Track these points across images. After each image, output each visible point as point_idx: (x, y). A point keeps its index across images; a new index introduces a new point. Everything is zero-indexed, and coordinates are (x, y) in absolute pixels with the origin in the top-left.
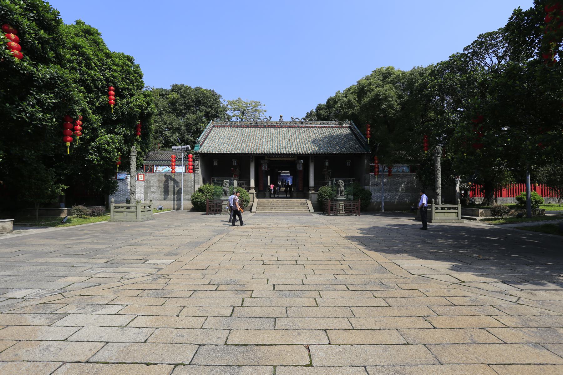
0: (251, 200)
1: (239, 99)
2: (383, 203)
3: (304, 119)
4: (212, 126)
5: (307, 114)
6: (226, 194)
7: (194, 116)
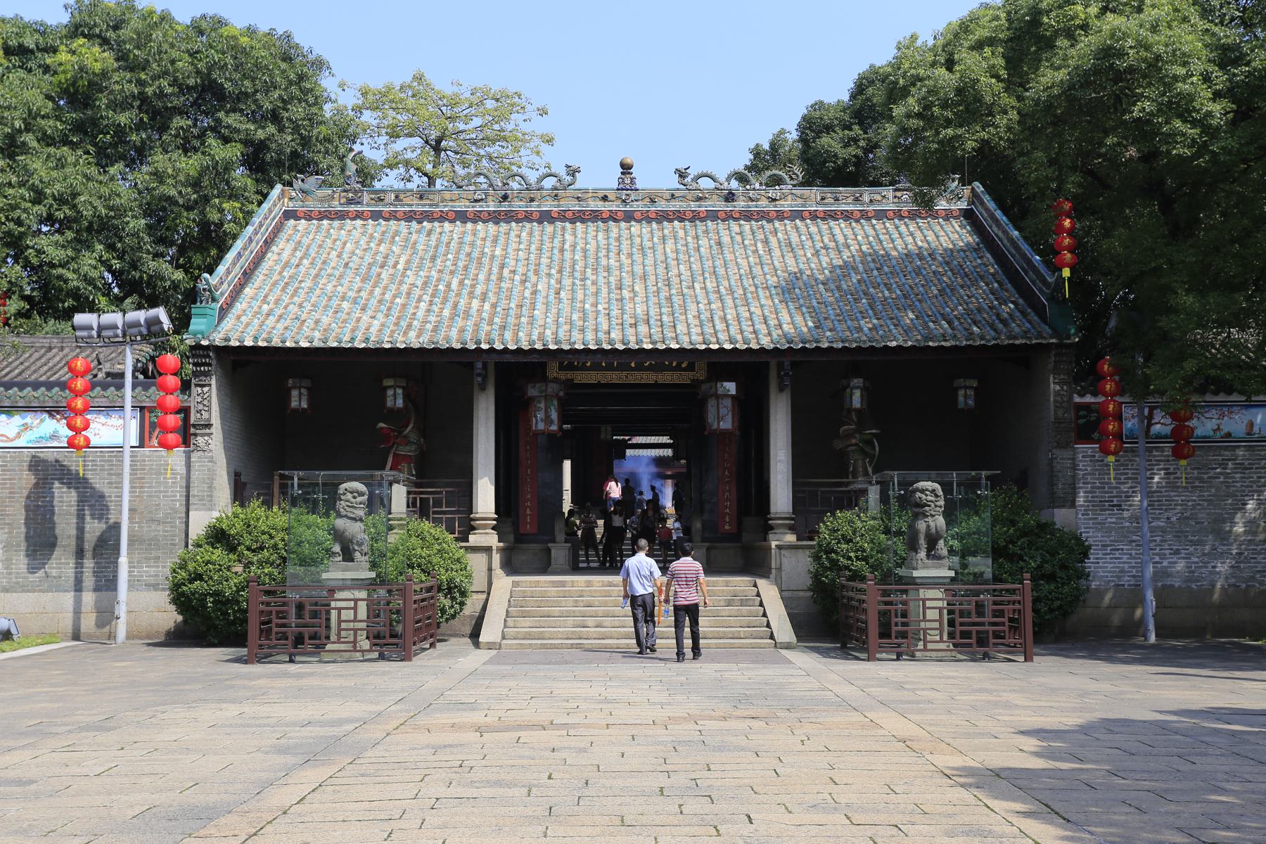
0: (479, 582)
1: (419, 78)
2: (1150, 595)
3: (742, 178)
4: (278, 211)
5: (757, 153)
6: (348, 555)
7: (190, 164)
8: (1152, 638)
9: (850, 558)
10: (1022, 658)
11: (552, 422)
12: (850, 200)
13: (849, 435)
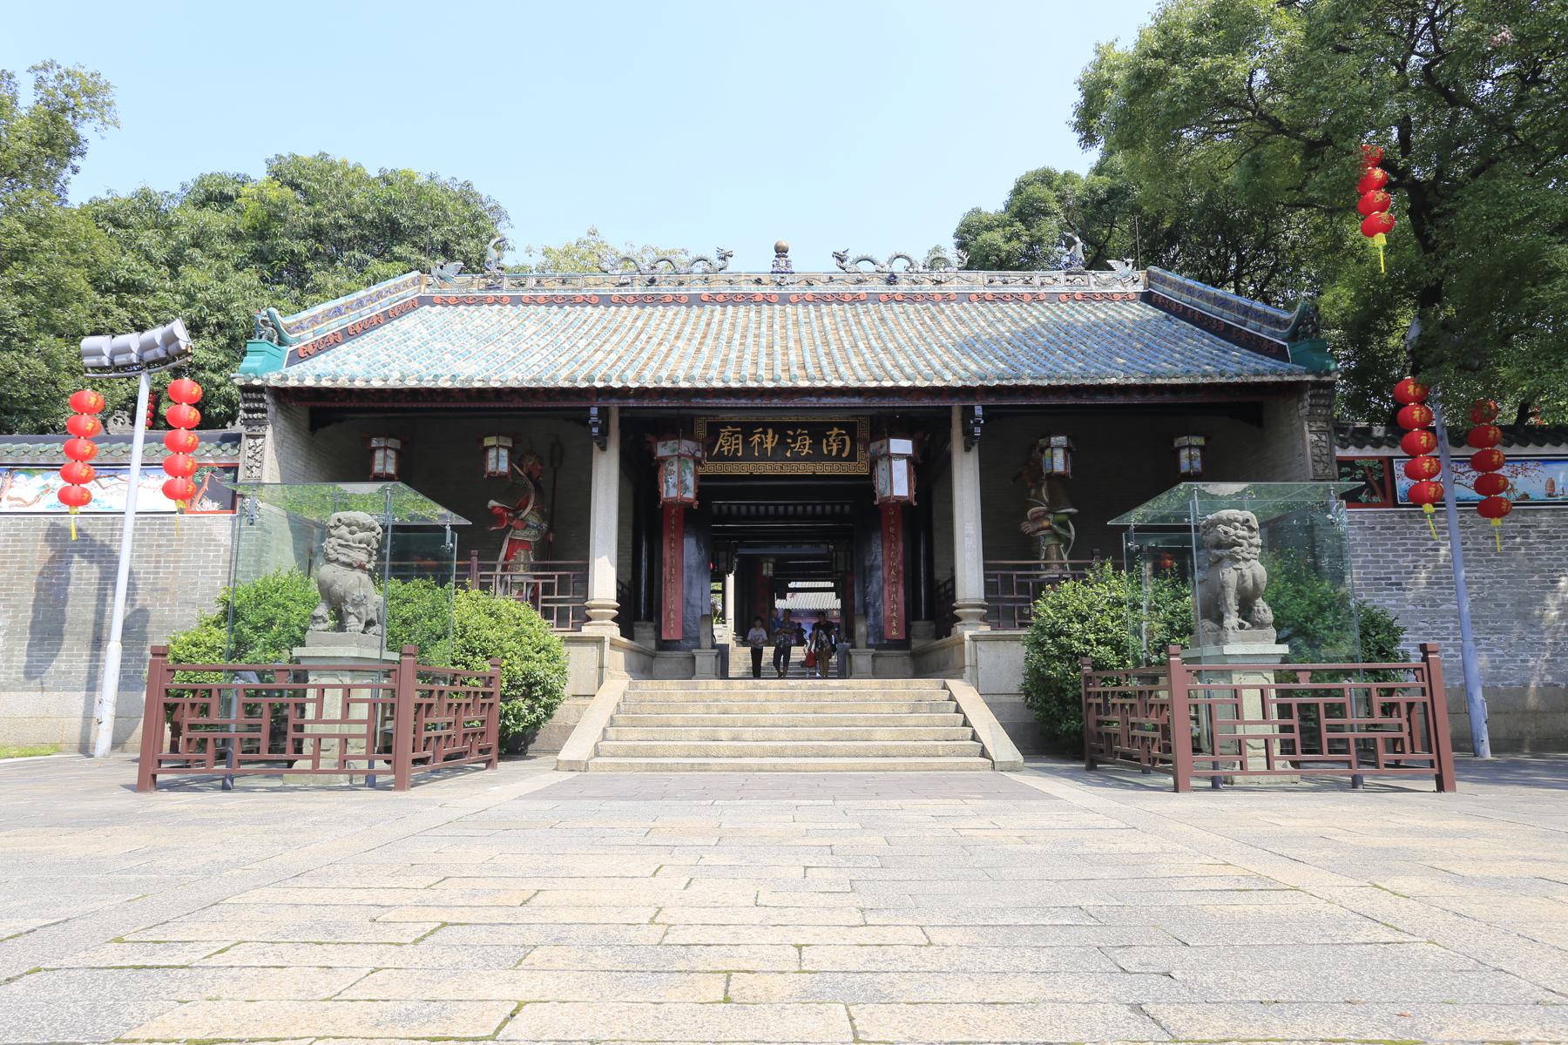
2: (1479, 696)
8: (1488, 756)
9: (1087, 642)
10: (1433, 785)
11: (687, 489)
13: (1037, 519)
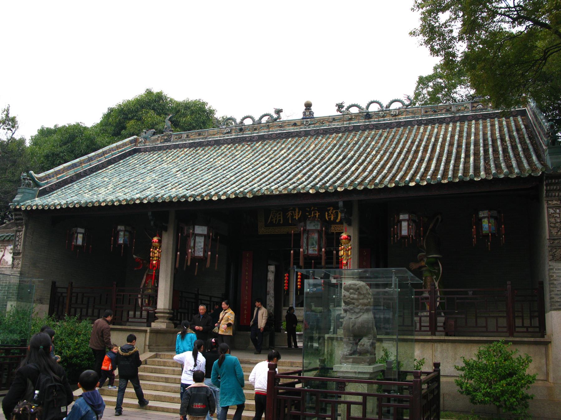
12: (443, 111)
